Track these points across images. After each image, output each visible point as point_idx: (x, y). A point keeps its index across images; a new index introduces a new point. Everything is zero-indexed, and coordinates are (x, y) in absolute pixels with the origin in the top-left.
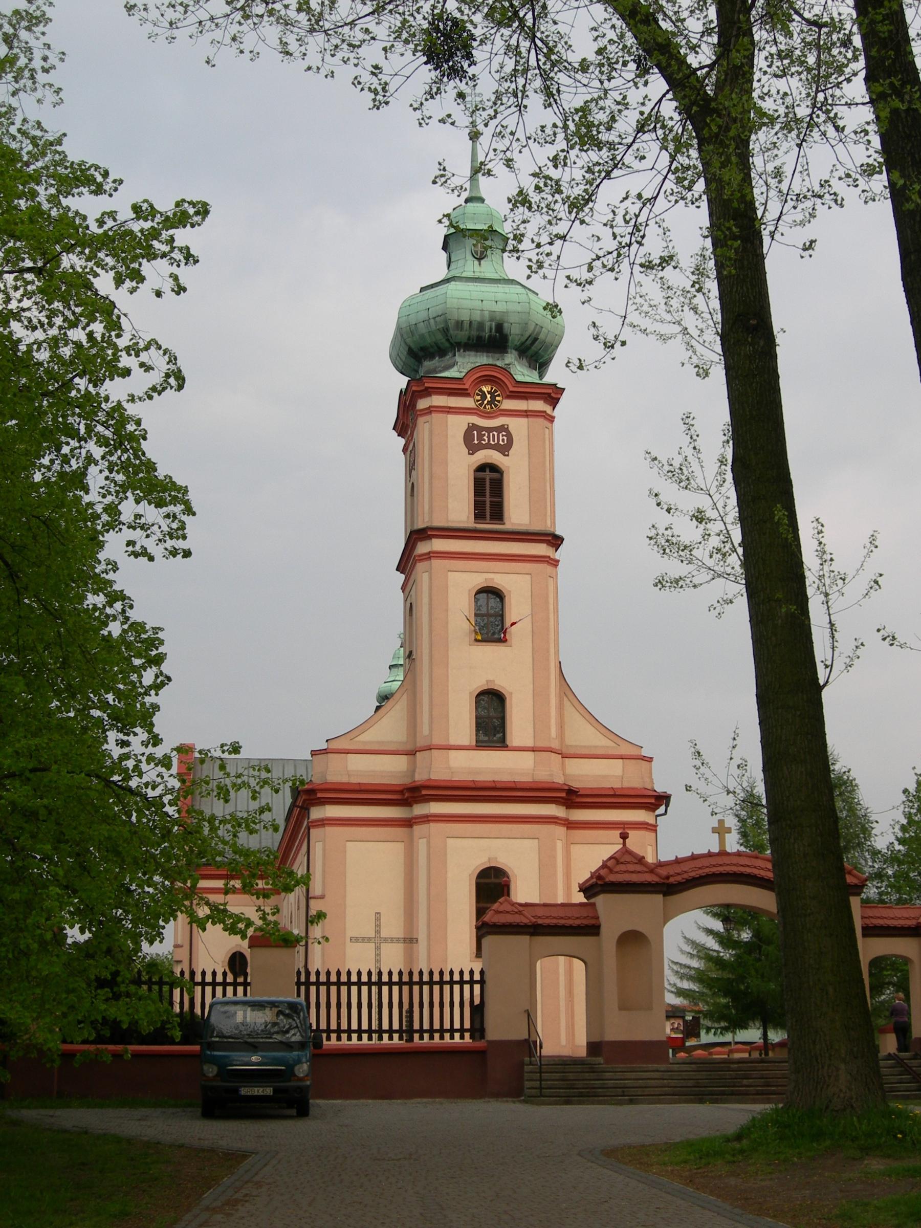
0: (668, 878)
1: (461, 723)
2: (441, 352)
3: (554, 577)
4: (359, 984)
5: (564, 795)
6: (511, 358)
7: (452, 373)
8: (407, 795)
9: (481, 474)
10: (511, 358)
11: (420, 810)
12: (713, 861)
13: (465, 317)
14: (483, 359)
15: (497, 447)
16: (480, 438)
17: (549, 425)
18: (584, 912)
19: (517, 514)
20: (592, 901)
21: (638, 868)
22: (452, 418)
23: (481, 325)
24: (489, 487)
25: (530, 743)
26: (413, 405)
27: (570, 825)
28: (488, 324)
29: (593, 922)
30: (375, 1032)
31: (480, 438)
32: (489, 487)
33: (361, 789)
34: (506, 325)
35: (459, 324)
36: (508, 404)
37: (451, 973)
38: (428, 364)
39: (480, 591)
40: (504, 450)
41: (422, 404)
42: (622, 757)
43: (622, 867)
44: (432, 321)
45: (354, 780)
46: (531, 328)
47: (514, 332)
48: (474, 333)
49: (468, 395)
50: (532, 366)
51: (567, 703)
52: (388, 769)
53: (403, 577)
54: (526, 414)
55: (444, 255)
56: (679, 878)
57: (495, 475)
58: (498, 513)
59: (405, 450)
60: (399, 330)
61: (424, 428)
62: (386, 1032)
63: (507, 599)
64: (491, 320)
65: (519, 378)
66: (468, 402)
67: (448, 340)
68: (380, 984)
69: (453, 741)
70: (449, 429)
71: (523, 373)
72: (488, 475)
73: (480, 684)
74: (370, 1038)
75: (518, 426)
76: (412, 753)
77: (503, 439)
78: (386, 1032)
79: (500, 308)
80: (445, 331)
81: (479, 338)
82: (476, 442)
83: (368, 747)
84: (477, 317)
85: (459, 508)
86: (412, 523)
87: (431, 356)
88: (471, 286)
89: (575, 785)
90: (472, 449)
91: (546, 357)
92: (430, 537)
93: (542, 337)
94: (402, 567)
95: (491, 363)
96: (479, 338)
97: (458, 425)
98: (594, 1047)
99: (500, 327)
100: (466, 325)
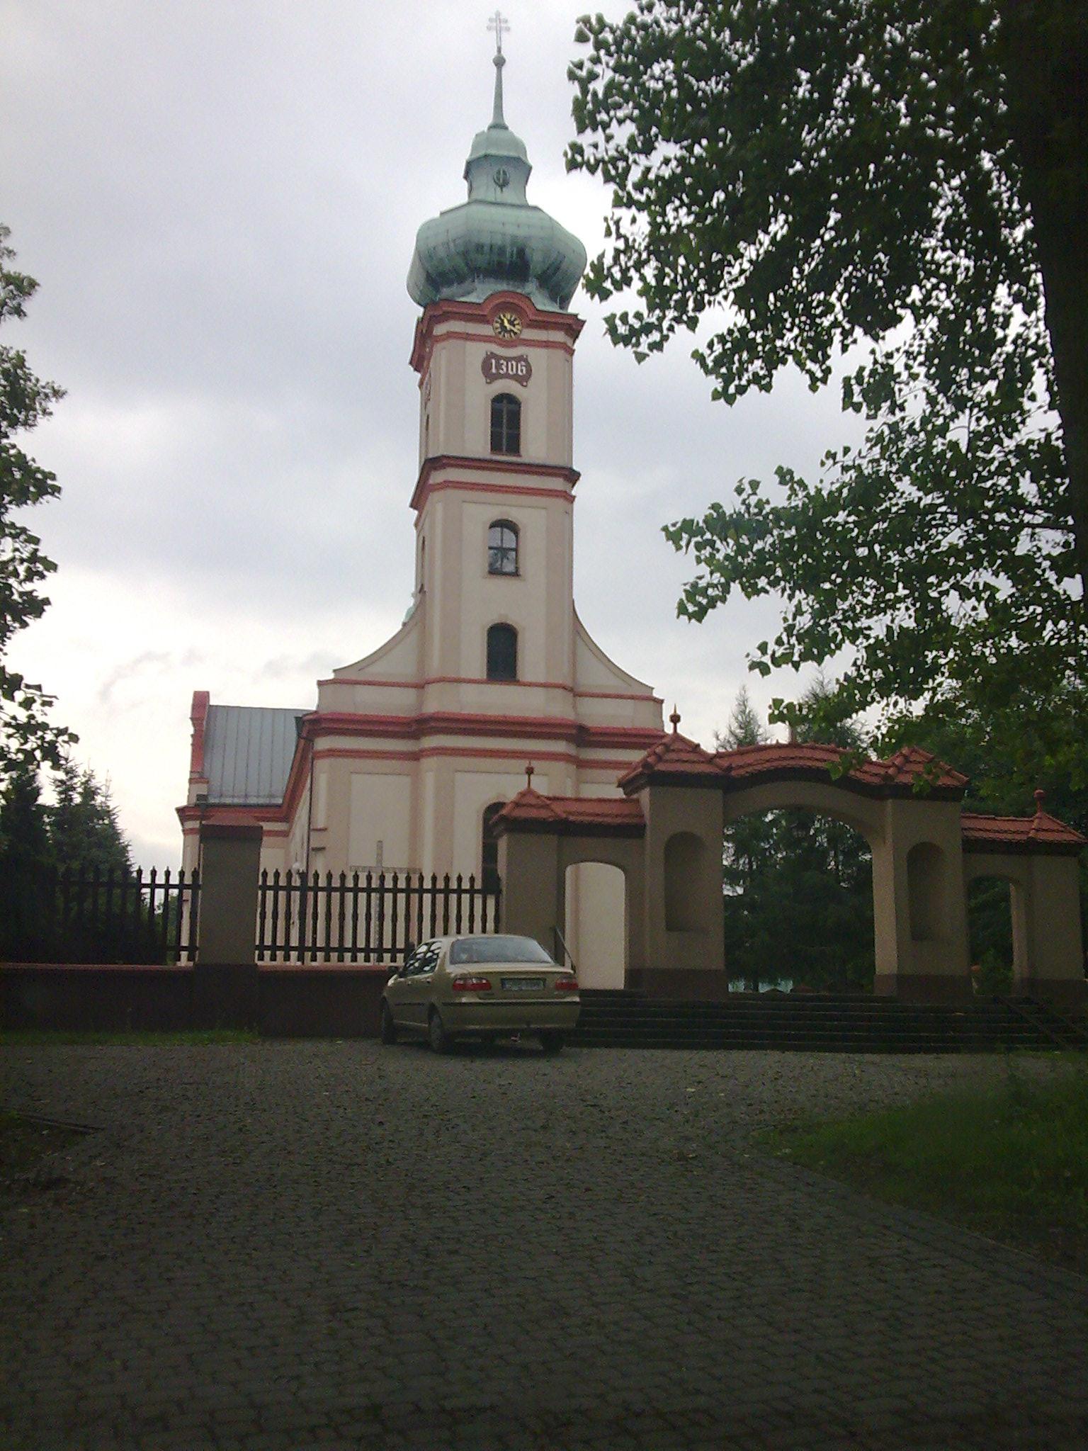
0: (730, 768)
1: (475, 659)
2: (461, 279)
3: (569, 513)
4: (356, 890)
5: (574, 732)
6: (531, 287)
7: (471, 298)
8: (414, 727)
9: (498, 406)
10: (531, 287)
11: (429, 742)
12: (783, 753)
13: (486, 240)
14: (502, 286)
15: (516, 378)
16: (499, 366)
17: (568, 356)
18: (626, 809)
19: (534, 447)
20: (635, 796)
21: (693, 757)
22: (470, 345)
23: (502, 250)
24: (506, 417)
25: (542, 681)
26: (430, 331)
27: (582, 764)
28: (508, 250)
29: (635, 821)
30: (374, 950)
31: (499, 366)
32: (506, 417)
33: (367, 720)
34: (527, 250)
35: (479, 248)
36: (529, 334)
37: (460, 879)
38: (446, 292)
39: (493, 526)
40: (523, 380)
41: (440, 329)
42: (632, 698)
43: (674, 756)
44: (452, 245)
45: (361, 712)
46: (554, 255)
47: (537, 260)
48: (496, 258)
49: (488, 322)
50: (553, 298)
51: (579, 641)
52: (398, 703)
53: (416, 512)
54: (547, 344)
55: (465, 184)
56: (742, 772)
57: (512, 407)
58: (514, 445)
59: (421, 385)
60: (418, 252)
61: (441, 355)
62: (387, 951)
63: (521, 534)
64: (513, 244)
65: (539, 307)
66: (487, 330)
67: (467, 264)
68: (382, 890)
69: (463, 675)
70: (464, 357)
71: (543, 303)
72: (505, 407)
73: (493, 618)
74: (367, 959)
75: (537, 356)
76: (420, 686)
77: (522, 370)
78: (387, 951)
79: (522, 232)
80: (465, 254)
81: (500, 264)
82: (494, 371)
83: (377, 679)
84: (498, 241)
85: (477, 442)
86: (427, 452)
87: (450, 283)
88: (493, 210)
89: (589, 723)
90: (490, 377)
91: (566, 291)
92: (444, 466)
93: (564, 266)
94: (417, 503)
95: (511, 289)
96: (500, 264)
97: (476, 352)
98: (633, 975)
99: (521, 252)
100: (486, 249)
